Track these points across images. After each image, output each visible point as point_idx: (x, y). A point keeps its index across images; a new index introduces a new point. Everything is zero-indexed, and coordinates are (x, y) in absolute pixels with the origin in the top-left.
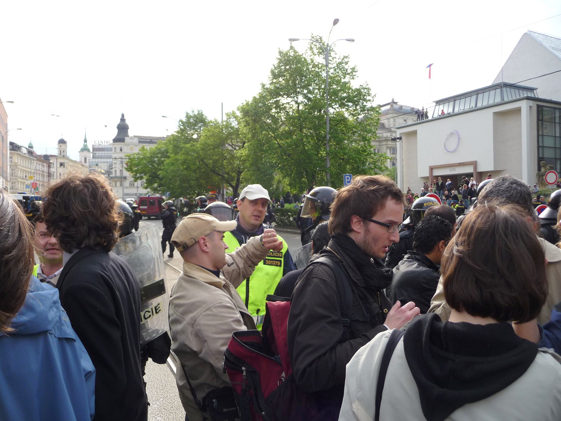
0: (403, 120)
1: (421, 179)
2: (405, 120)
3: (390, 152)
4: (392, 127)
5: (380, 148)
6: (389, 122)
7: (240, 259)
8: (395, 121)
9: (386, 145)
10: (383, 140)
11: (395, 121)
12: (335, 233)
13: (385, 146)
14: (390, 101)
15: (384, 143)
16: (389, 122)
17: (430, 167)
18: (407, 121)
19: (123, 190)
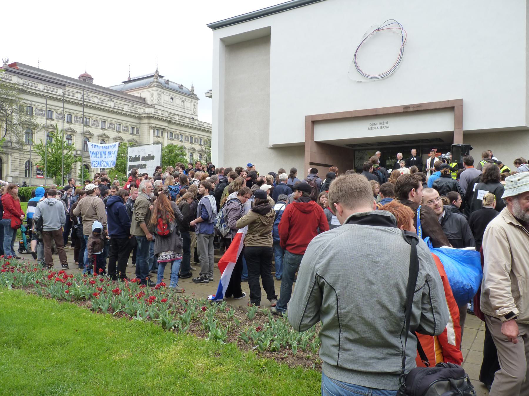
0: (170, 97)
1: (271, 151)
2: (172, 98)
3: (154, 134)
4: (155, 104)
5: (140, 128)
6: (152, 97)
7: (96, 200)
8: (159, 97)
9: (148, 123)
10: (145, 117)
11: (159, 97)
12: (227, 235)
13: (147, 124)
14: (152, 72)
15: (146, 121)
16: (152, 97)
17: (307, 117)
18: (174, 99)
19: (80, 150)
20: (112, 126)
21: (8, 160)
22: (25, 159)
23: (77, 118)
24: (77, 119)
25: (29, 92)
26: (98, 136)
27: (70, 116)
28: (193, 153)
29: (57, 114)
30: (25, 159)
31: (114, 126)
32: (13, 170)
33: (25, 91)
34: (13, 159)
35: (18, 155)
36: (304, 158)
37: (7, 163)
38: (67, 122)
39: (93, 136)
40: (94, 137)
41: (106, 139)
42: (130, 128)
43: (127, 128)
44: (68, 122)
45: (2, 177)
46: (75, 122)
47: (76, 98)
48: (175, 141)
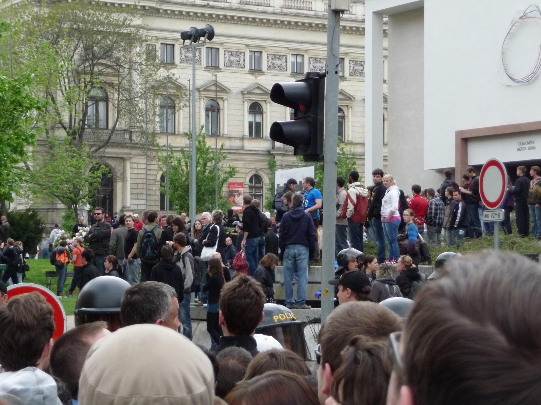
20: (237, 59)
21: (124, 173)
22: (248, 170)
23: (274, 59)
24: (274, 62)
25: (166, 11)
26: (243, 93)
27: (257, 55)
28: (345, 109)
29: (227, 55)
30: (248, 170)
31: (242, 57)
32: (136, 196)
33: (158, 10)
34: (136, 171)
35: (144, 161)
36: (364, 35)
37: (124, 180)
38: (293, 73)
39: (227, 93)
40: (354, 104)
41: (345, 103)
42: (248, 54)
43: (280, 59)
44: (208, 68)
45: (114, 212)
46: (269, 68)
47: (270, 10)
48: (352, 83)
